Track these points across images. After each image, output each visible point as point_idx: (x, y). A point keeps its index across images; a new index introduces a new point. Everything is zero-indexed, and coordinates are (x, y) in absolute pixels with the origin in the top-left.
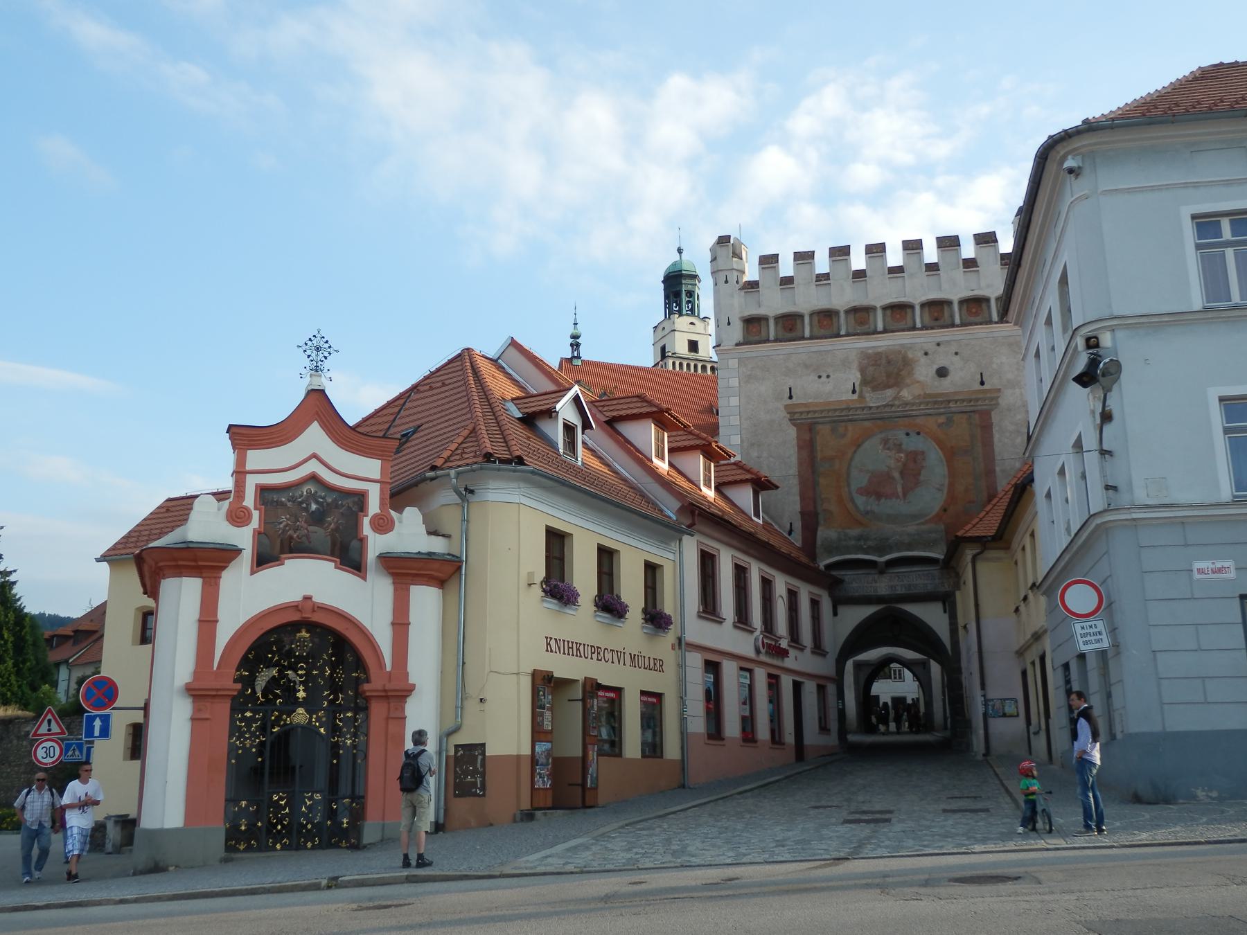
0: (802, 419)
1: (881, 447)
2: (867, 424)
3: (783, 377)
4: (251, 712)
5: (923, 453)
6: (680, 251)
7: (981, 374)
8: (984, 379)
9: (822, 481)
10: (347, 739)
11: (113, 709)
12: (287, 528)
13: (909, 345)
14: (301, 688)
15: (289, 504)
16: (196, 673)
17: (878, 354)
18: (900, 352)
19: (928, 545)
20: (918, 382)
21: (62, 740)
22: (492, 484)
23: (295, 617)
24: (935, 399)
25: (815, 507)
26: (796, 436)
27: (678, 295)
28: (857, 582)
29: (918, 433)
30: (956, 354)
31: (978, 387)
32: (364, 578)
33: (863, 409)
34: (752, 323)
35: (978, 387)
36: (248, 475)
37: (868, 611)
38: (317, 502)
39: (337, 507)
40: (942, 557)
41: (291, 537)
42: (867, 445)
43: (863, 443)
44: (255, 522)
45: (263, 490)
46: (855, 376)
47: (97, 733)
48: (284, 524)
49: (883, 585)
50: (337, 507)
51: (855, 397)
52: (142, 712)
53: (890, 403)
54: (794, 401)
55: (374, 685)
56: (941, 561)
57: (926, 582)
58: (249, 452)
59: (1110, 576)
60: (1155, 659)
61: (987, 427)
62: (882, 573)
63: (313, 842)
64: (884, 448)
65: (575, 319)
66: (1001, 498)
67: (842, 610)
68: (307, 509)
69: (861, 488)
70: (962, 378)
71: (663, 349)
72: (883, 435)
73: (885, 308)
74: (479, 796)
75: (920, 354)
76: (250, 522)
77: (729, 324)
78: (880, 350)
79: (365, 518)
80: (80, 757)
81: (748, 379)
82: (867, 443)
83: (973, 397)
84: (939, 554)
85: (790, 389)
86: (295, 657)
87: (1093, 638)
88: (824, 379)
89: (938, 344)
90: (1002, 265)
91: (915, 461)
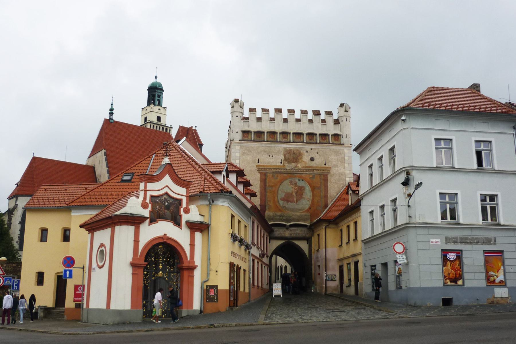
0: (262, 171)
1: (289, 184)
2: (285, 175)
3: (256, 155)
4: (146, 272)
5: (304, 187)
6: (156, 77)
7: (325, 161)
8: (326, 163)
9: (268, 194)
10: (174, 282)
11: (73, 268)
12: (159, 210)
13: (301, 148)
14: (161, 265)
15: (159, 202)
16: (133, 259)
17: (290, 150)
18: (298, 150)
19: (304, 220)
20: (304, 162)
21: (4, 277)
22: (221, 200)
23: (161, 241)
24: (309, 169)
25: (265, 204)
26: (259, 177)
27: (154, 96)
28: (278, 232)
29: (303, 180)
30: (317, 153)
31: (324, 166)
32: (181, 229)
33: (284, 169)
34: (246, 133)
35: (324, 166)
36: (148, 192)
37: (280, 242)
38: (167, 202)
39: (173, 204)
40: (309, 225)
41: (160, 214)
42: (285, 182)
43: (284, 181)
44: (150, 208)
45: (152, 197)
46: (282, 157)
47: (68, 276)
48: (158, 209)
49: (287, 234)
50: (173, 204)
51: (282, 165)
52: (82, 269)
53: (294, 168)
54: (260, 164)
55: (185, 264)
56: (308, 226)
57: (302, 233)
58: (148, 183)
59: (407, 242)
60: (419, 267)
61: (326, 180)
62: (287, 229)
63: (165, 315)
64: (291, 184)
65: (112, 102)
66: (333, 207)
67: (272, 241)
68: (164, 204)
69: (282, 198)
70: (318, 162)
71: (146, 119)
72: (290, 180)
73: (293, 134)
74: (216, 302)
75: (305, 152)
76: (148, 208)
77: (237, 132)
78: (291, 149)
79: (182, 208)
80: (10, 284)
81: (243, 154)
82: (285, 182)
83: (322, 169)
84: (308, 223)
85: (258, 159)
86: (159, 254)
87: (402, 260)
88: (271, 157)
89: (311, 149)
90: (334, 123)
91: (301, 190)
